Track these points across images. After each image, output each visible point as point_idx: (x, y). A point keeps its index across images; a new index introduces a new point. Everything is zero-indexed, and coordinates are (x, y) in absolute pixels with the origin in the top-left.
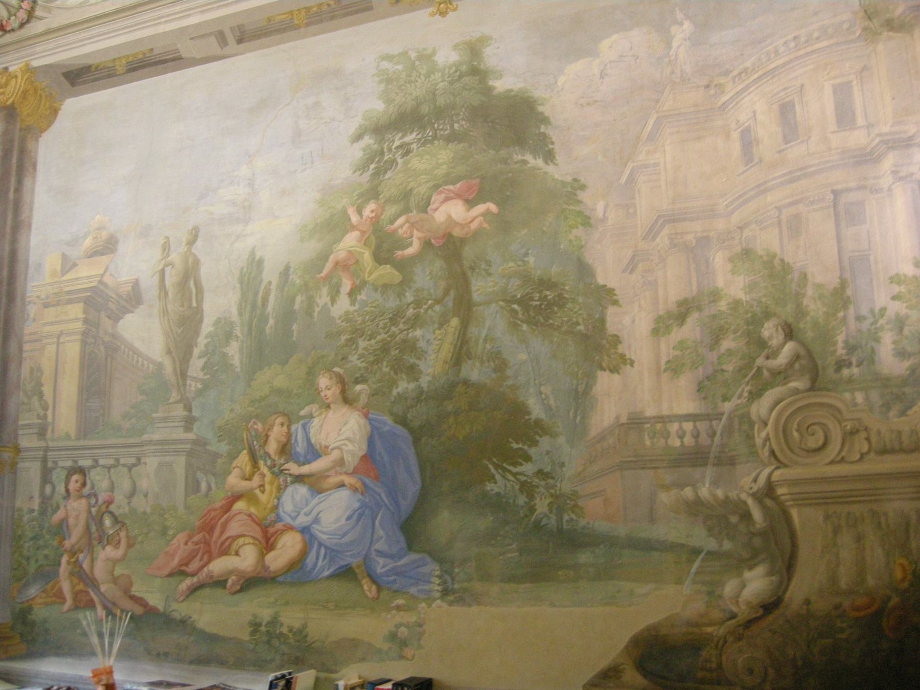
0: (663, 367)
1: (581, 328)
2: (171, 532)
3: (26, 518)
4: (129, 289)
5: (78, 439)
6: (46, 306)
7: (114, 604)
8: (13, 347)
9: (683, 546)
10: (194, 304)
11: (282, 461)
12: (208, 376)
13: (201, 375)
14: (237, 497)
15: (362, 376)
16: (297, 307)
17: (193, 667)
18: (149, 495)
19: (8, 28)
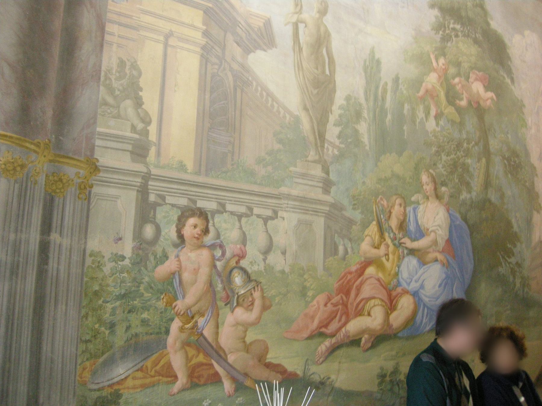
2: (310, 293)
4: (261, 25)
10: (327, 72)
13: (337, 142)
16: (405, 112)
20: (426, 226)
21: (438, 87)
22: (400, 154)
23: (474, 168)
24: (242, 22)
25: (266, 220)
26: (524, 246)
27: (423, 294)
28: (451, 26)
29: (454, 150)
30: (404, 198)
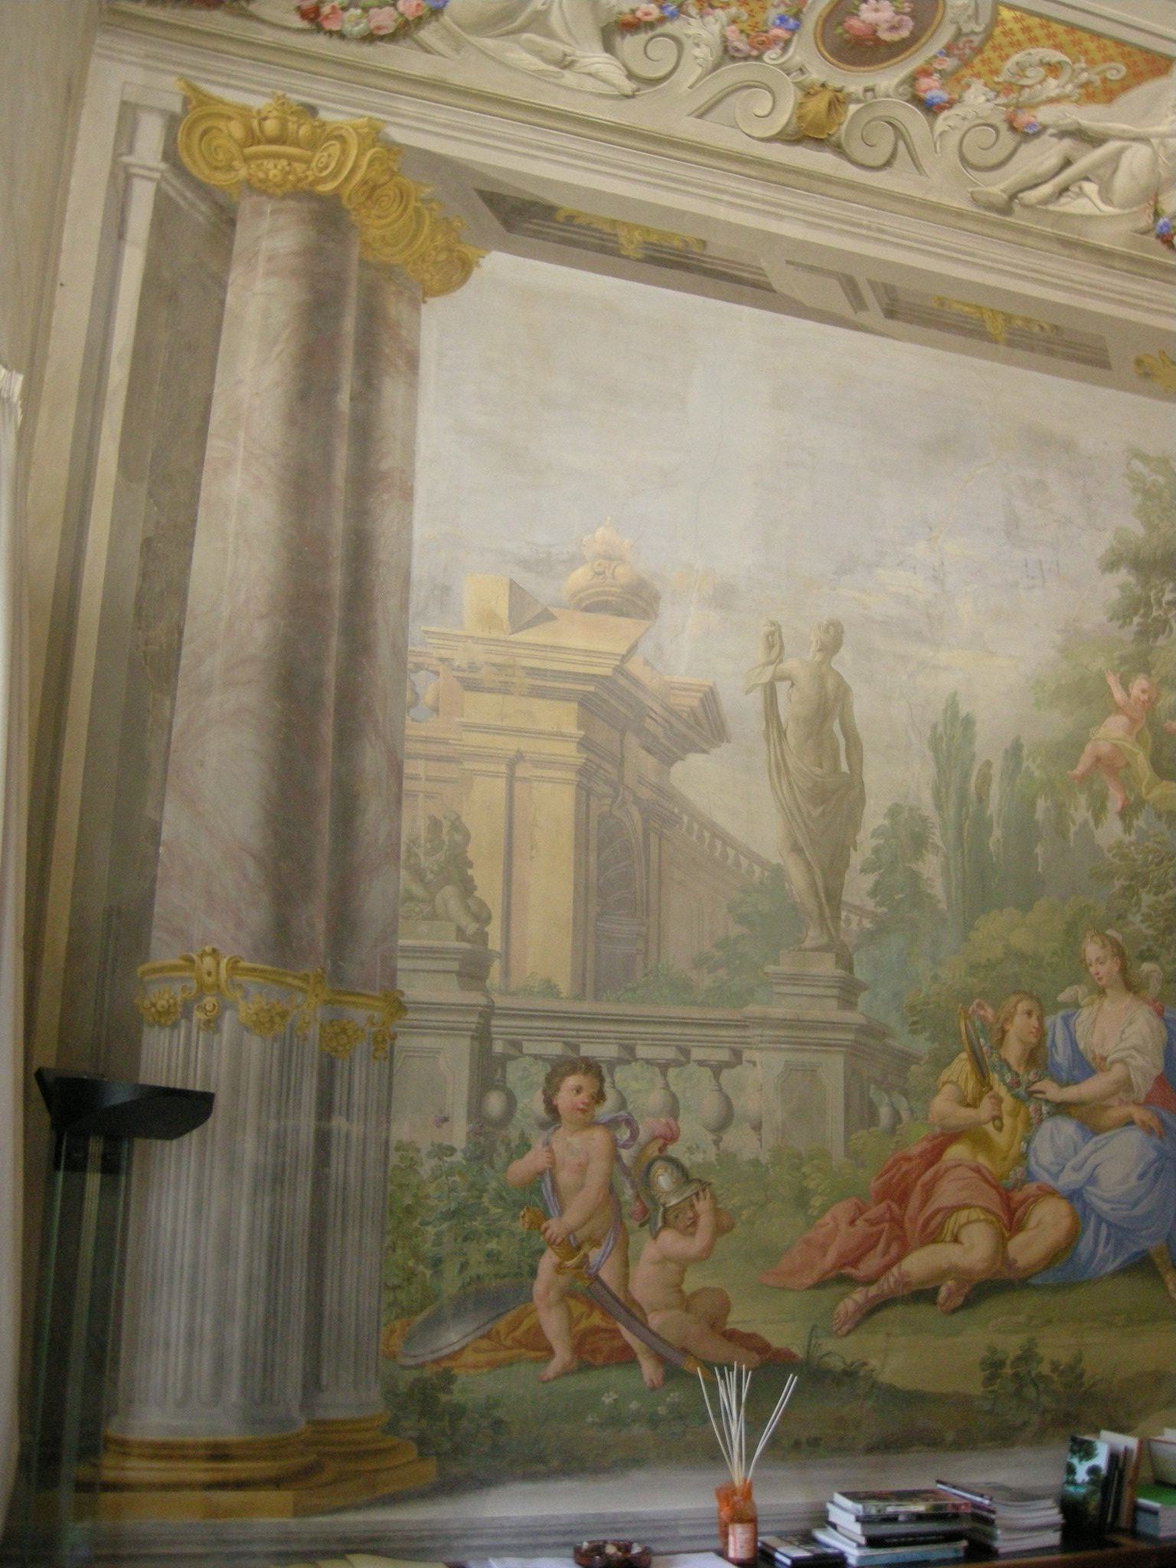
2: (817, 1202)
3: (426, 1169)
4: (696, 703)
5: (580, 997)
6: (472, 686)
7: (685, 1351)
8: (371, 758)
10: (844, 767)
11: (1032, 1076)
12: (884, 909)
13: (870, 904)
14: (952, 1137)
15: (1149, 949)
16: (1039, 815)
17: (873, 1458)
18: (765, 1128)
19: (329, 25)
21: (1129, 745)
22: (1026, 906)
25: (717, 1069)
30: (1038, 1000)
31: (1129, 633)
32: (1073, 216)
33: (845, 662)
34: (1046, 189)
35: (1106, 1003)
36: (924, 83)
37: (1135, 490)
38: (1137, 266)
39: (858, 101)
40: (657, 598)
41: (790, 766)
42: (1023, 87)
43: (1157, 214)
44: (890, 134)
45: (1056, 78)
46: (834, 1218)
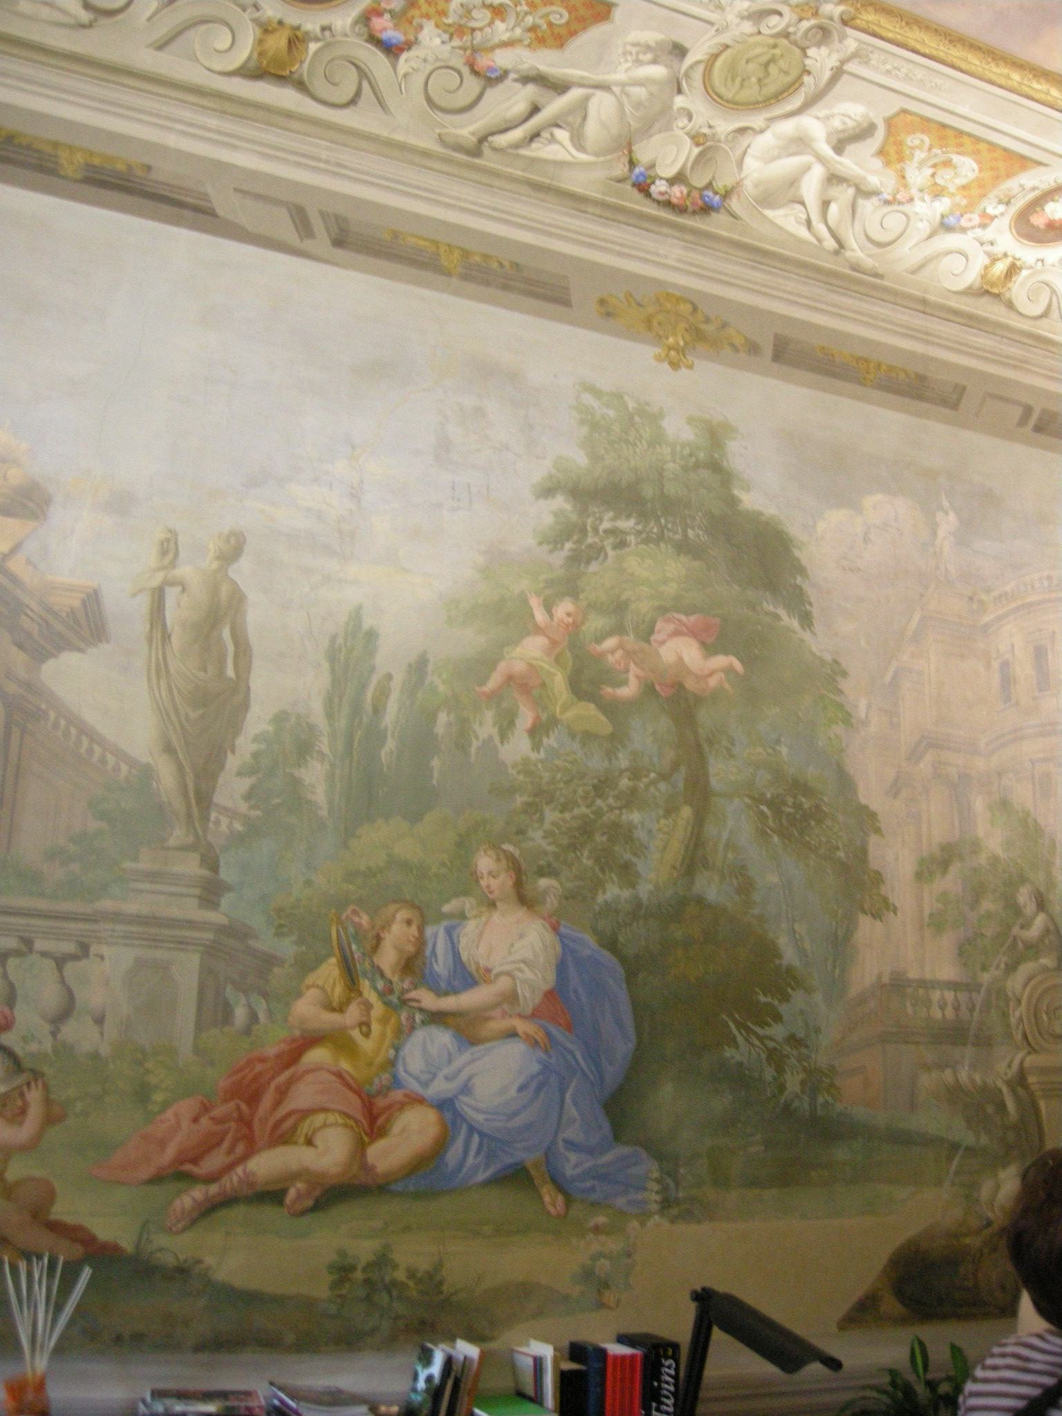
0: (926, 920)
1: (841, 854)
2: (158, 1097)
4: (77, 603)
9: (942, 1140)
10: (230, 672)
11: (406, 985)
12: (258, 813)
13: (243, 807)
15: (549, 865)
16: (440, 729)
17: (203, 1357)
20: (483, 963)
21: (547, 665)
22: (415, 817)
23: (650, 831)
24: (34, 605)
25: (60, 961)
26: (818, 997)
27: (468, 1106)
28: (606, 525)
29: (585, 798)
30: (419, 909)
31: (558, 558)
32: (546, 161)
33: (243, 572)
34: (517, 134)
35: (496, 917)
36: (377, 23)
37: (582, 422)
38: (610, 211)
39: (317, 39)
40: (48, 501)
41: (172, 670)
42: (473, 30)
43: (632, 164)
44: (353, 74)
45: (503, 21)
46: (176, 1114)
